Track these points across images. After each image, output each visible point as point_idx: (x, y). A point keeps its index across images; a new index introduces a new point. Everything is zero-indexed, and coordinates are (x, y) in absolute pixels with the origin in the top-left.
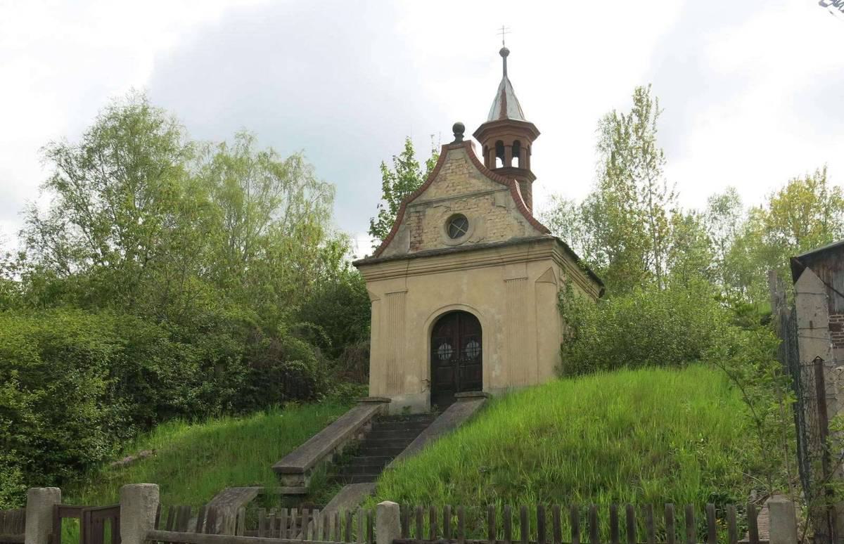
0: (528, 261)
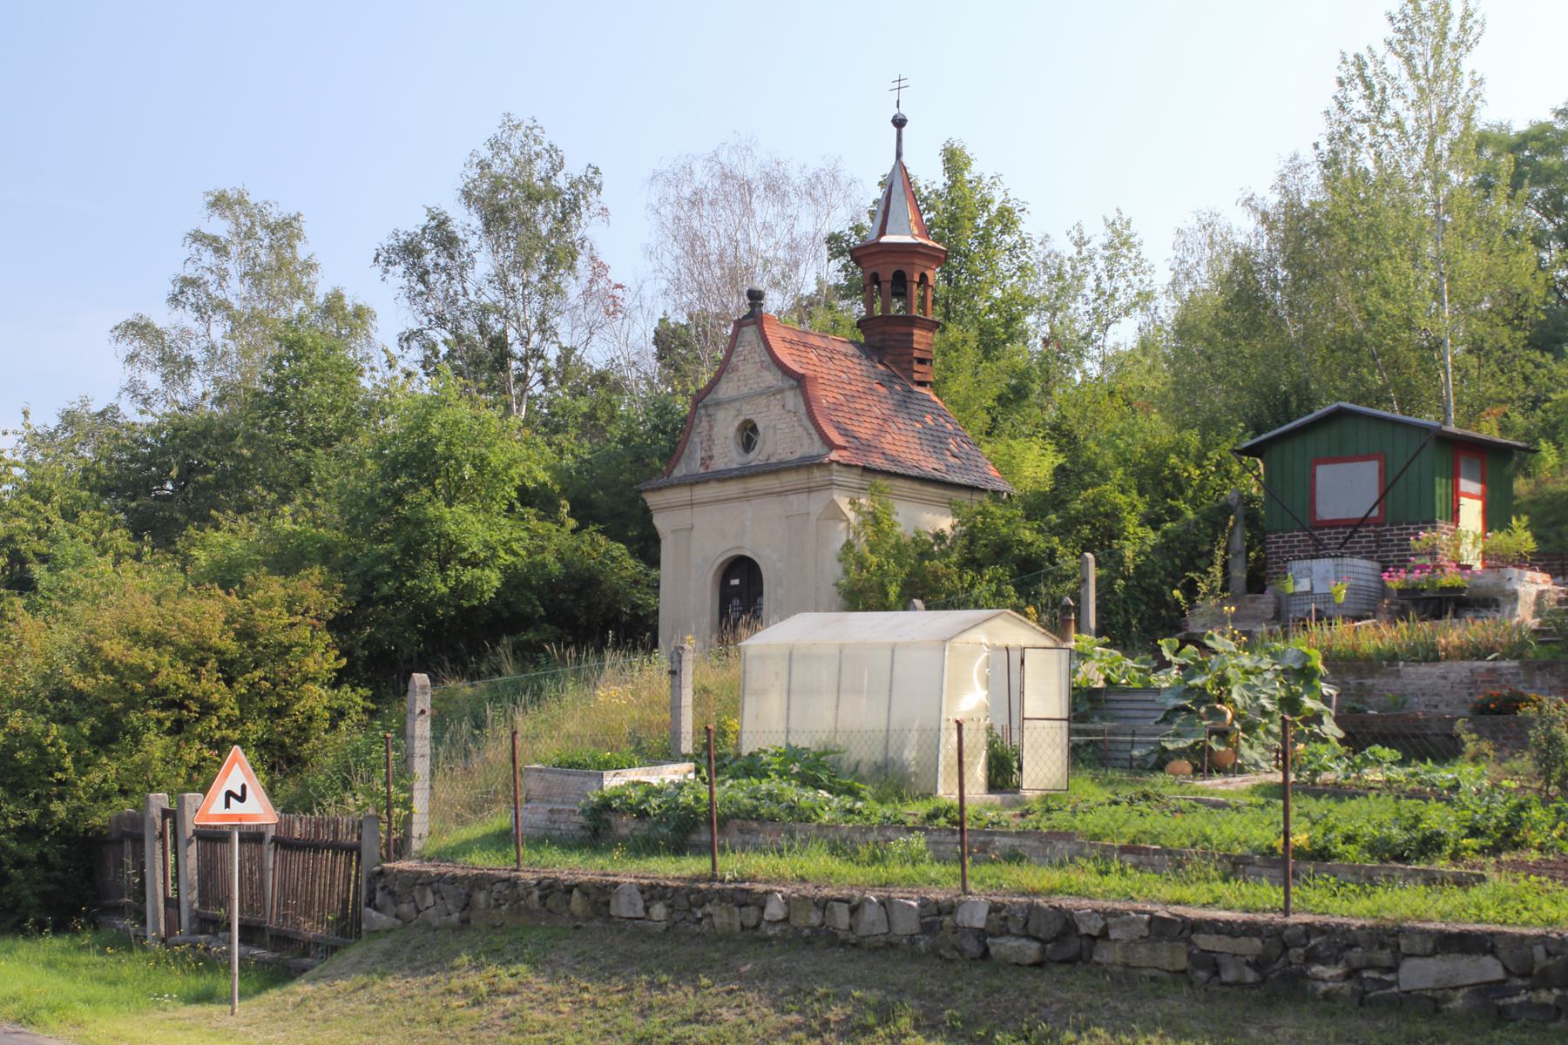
0: (810, 490)
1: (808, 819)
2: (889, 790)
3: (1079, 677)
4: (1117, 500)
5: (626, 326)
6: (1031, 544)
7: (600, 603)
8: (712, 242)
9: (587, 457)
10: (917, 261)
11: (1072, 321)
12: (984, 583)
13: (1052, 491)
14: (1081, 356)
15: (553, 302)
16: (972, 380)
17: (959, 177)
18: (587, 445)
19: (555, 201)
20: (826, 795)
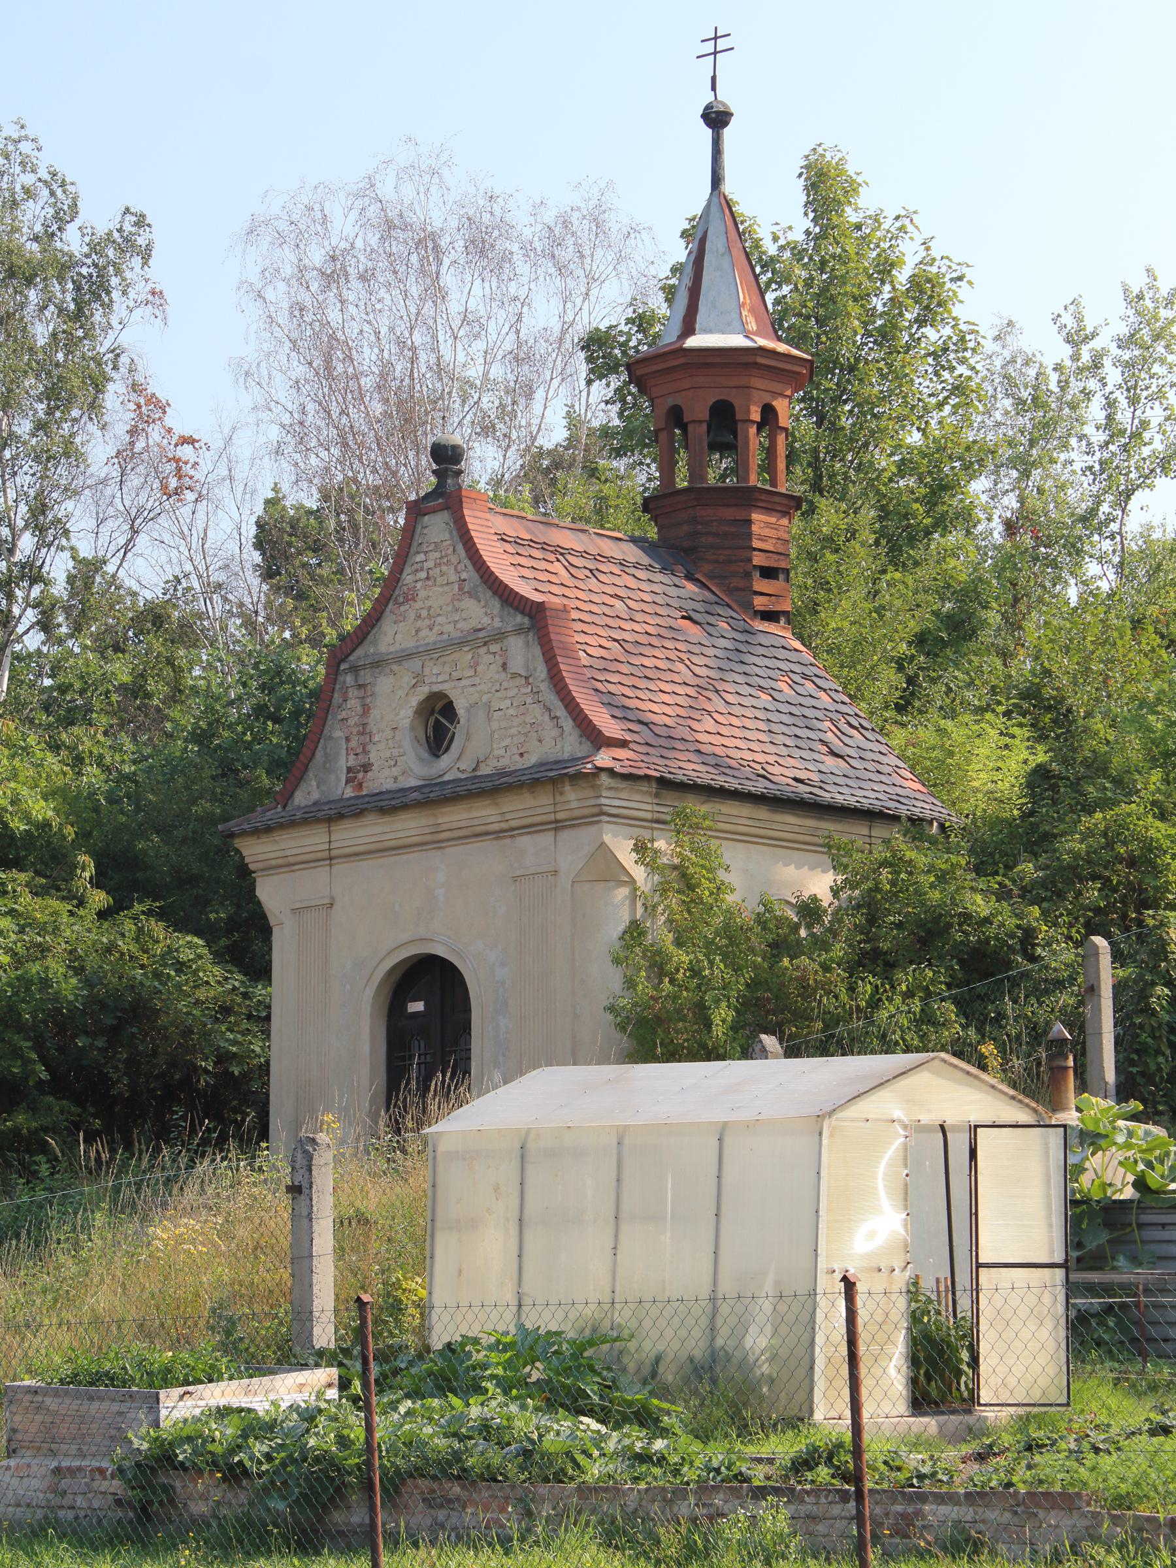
0: (557, 826)
1: (560, 1477)
2: (718, 1413)
3: (1085, 1180)
4: (1152, 833)
5: (201, 514)
6: (987, 921)
7: (155, 1053)
8: (367, 350)
9: (127, 769)
10: (756, 382)
11: (1062, 488)
12: (898, 1000)
13: (1025, 816)
14: (1079, 552)
15: (62, 473)
16: (868, 606)
17: (835, 220)
18: (129, 746)
19: (61, 279)
20: (595, 1425)
